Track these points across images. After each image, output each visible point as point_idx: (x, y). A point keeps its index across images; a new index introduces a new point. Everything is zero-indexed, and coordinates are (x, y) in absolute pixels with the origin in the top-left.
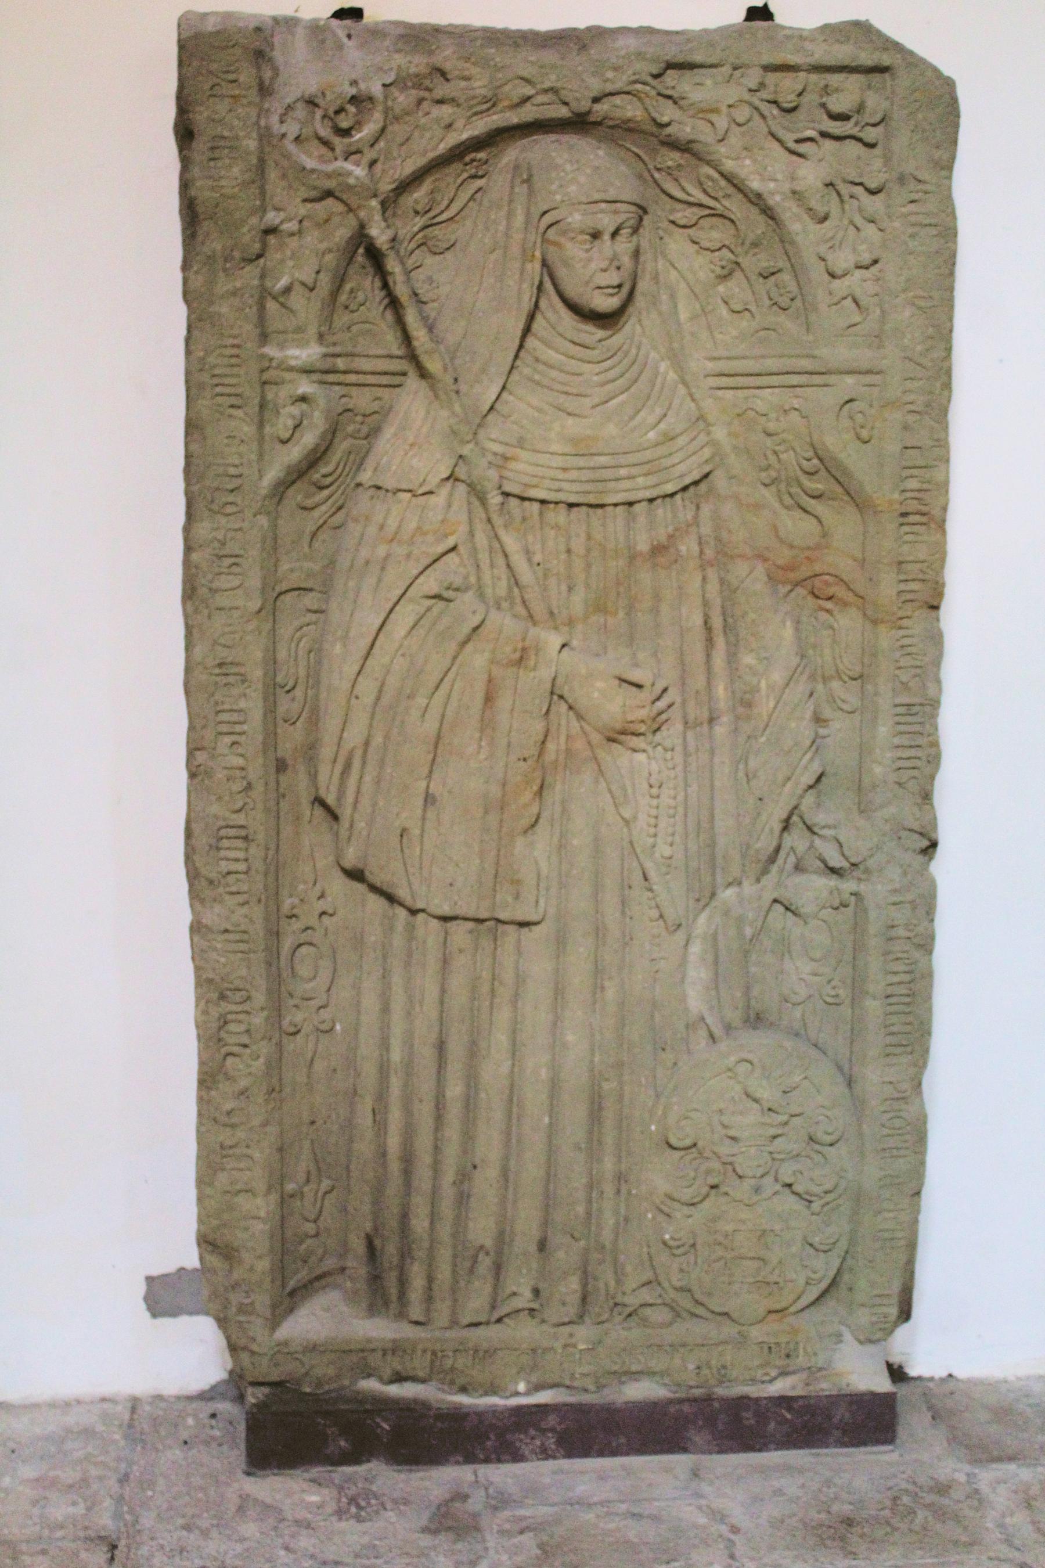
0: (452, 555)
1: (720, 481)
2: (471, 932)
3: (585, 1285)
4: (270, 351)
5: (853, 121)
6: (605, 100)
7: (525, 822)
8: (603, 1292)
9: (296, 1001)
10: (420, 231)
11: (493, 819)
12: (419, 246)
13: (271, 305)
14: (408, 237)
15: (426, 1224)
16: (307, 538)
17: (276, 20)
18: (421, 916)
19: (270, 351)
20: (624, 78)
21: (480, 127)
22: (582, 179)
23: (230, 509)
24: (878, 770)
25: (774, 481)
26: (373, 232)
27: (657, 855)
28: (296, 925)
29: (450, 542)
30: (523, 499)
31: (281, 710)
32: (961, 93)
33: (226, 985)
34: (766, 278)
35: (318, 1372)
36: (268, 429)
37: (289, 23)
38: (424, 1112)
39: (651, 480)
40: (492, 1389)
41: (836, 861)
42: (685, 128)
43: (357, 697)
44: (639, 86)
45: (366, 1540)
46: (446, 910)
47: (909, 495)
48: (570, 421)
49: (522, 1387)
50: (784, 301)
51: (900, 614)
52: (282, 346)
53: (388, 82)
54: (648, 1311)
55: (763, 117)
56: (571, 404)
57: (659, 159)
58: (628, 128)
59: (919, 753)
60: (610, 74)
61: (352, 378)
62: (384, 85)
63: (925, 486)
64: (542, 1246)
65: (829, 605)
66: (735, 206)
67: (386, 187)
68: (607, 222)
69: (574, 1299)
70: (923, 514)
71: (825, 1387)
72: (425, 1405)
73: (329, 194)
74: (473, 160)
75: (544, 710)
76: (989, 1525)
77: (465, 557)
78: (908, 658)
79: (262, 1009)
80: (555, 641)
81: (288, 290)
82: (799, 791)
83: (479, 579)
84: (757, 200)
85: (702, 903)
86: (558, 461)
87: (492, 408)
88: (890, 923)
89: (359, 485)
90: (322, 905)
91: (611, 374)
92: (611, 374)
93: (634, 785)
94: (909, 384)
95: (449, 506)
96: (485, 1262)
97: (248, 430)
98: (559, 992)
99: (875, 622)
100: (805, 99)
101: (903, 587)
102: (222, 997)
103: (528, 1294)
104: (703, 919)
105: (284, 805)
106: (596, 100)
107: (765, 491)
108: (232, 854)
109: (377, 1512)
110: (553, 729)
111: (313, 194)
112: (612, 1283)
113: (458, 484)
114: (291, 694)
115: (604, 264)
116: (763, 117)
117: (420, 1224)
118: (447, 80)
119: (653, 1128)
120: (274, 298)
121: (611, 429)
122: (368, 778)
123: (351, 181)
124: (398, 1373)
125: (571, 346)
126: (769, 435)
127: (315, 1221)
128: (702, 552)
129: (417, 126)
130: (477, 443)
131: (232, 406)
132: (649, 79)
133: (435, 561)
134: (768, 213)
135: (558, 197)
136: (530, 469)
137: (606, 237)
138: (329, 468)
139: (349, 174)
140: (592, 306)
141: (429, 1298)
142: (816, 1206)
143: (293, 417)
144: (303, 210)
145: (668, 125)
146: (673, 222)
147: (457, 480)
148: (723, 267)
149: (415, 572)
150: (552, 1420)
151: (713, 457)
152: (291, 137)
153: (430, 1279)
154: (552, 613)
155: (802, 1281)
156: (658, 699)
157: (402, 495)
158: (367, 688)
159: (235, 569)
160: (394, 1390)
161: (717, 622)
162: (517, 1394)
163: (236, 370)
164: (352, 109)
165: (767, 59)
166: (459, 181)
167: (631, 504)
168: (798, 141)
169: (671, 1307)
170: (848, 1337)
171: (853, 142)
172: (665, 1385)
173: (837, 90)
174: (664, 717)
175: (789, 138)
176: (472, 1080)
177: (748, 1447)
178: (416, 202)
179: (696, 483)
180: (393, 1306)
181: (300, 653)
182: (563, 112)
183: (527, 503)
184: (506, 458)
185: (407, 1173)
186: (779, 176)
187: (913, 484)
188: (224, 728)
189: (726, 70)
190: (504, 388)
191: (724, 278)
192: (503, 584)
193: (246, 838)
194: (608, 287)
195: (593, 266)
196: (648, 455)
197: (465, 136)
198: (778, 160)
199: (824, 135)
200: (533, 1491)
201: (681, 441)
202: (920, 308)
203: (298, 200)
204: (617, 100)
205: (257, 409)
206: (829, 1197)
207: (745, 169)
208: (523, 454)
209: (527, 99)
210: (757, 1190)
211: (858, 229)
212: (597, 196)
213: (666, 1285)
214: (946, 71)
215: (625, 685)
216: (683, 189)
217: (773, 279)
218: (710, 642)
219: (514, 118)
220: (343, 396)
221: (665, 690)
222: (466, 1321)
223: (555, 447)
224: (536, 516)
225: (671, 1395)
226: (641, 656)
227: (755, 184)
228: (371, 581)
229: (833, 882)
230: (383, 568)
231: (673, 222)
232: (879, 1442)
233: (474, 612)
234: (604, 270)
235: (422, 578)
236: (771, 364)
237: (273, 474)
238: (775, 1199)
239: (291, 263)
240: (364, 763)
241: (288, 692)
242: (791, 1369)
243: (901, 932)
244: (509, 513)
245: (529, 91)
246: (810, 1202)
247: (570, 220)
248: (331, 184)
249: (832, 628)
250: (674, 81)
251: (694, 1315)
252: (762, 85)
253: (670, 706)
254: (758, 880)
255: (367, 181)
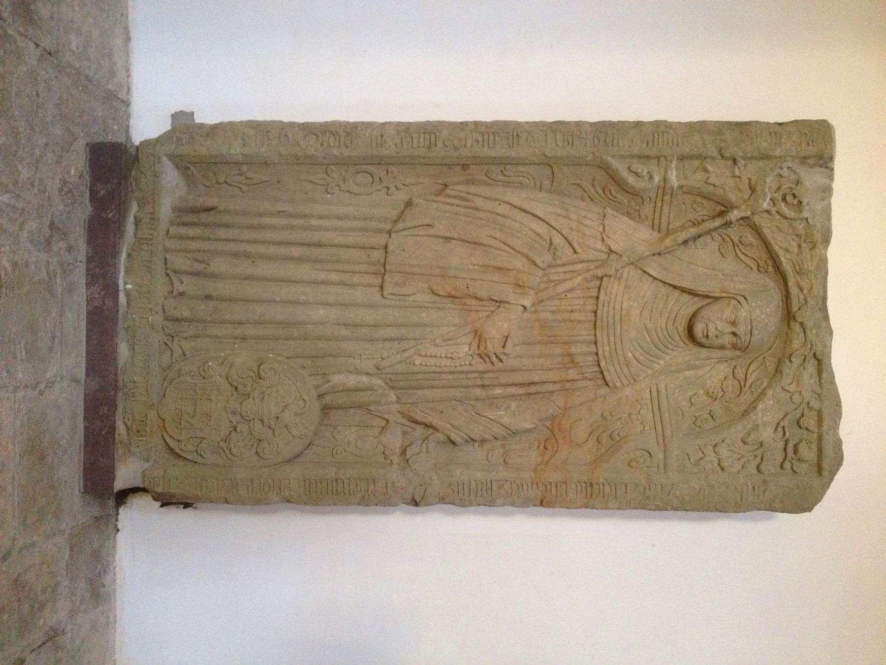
0: (572, 251)
1: (604, 391)
2: (379, 261)
3: (186, 320)
4: (674, 162)
5: (794, 456)
6: (802, 329)
7: (435, 288)
8: (181, 329)
9: (343, 173)
10: (732, 240)
11: (437, 272)
12: (723, 239)
13: (697, 163)
14: (729, 234)
15: (223, 237)
16: (577, 182)
17: (832, 169)
18: (387, 236)
19: (674, 162)
20: (813, 339)
21: (787, 266)
22: (763, 317)
23: (596, 140)
24: (458, 472)
25: (605, 419)
26: (735, 212)
27: (415, 357)
28: (383, 174)
29: (579, 250)
30: (599, 288)
31: (492, 167)
32: (806, 514)
33: (354, 136)
34: (710, 414)
35: (143, 180)
36: (635, 160)
37: (831, 177)
38: (285, 236)
39: (607, 354)
40: (127, 272)
41: (409, 453)
42: (789, 369)
43: (500, 204)
44: (809, 346)
45: (48, 188)
46: (391, 248)
47: (602, 487)
48: (638, 312)
49: (129, 286)
50: (698, 423)
51: (540, 484)
52: (677, 168)
53: (809, 220)
54: (169, 353)
55: (796, 409)
56: (646, 313)
57: (770, 358)
58: (788, 340)
59: (467, 494)
60: (814, 331)
61: (659, 204)
62: (807, 218)
63: (606, 496)
64: (208, 297)
65: (542, 447)
66: (747, 398)
67: (757, 219)
68: (741, 330)
69: (177, 314)
70: (591, 495)
71: (120, 452)
72: (121, 236)
73: (753, 191)
74: (768, 265)
75: (493, 298)
76: (35, 538)
77: (571, 258)
78: (516, 488)
79: (341, 154)
80: (527, 303)
81: (706, 170)
82: (447, 432)
83: (558, 266)
84: (752, 407)
85: (390, 383)
86: (618, 306)
87: (644, 272)
88: (376, 480)
89: (605, 208)
90: (393, 189)
91: (660, 334)
92: (660, 334)
93: (452, 345)
94: (659, 487)
95: (596, 250)
96: (200, 267)
97: (636, 150)
98: (346, 305)
99: (535, 470)
100: (804, 432)
101: (554, 485)
102: (348, 134)
103: (181, 290)
104: (380, 382)
105: (445, 168)
106: (802, 324)
107: (599, 414)
108: (422, 139)
109: (63, 201)
110: (483, 303)
111: (753, 183)
112: (185, 335)
113: (607, 255)
114: (500, 173)
115: (719, 328)
116: (796, 409)
117: (223, 233)
118: (811, 249)
119: (271, 356)
120: (701, 164)
121: (633, 334)
122: (459, 209)
123: (761, 201)
124: (140, 221)
125: (675, 314)
126: (629, 415)
127: (225, 182)
128: (568, 381)
129: (787, 235)
130: (628, 264)
131: (648, 142)
132: (813, 351)
133: (569, 243)
134: (746, 413)
135: (754, 304)
136: (614, 291)
137: (733, 329)
138: (613, 193)
139: (764, 200)
140: (697, 323)
141: (181, 238)
142: (222, 444)
143: (642, 172)
144: (745, 179)
145: (790, 361)
146: (735, 367)
147: (609, 254)
148: (713, 393)
149: (564, 232)
150: (109, 303)
151: (616, 387)
152: (781, 172)
153: (192, 239)
154: (541, 302)
155: (181, 438)
156: (497, 357)
157: (602, 227)
158: (503, 209)
159: (566, 143)
160: (131, 219)
161: (533, 389)
162: (125, 283)
163: (665, 143)
164: (796, 202)
165: (825, 411)
166: (756, 259)
167: (596, 343)
168: (783, 427)
169: (170, 367)
170: (147, 465)
171: (783, 457)
172: (126, 364)
173: (810, 448)
174: (487, 360)
175: (784, 423)
176: (300, 260)
177: (86, 410)
178: (747, 237)
179: (604, 379)
180: (178, 220)
181: (521, 178)
182: (795, 308)
183: (597, 290)
184: (620, 279)
185: (251, 227)
186: (765, 419)
187: (607, 489)
188: (486, 137)
189: (818, 390)
190: (655, 278)
191: (707, 394)
192: (555, 277)
193: (430, 147)
194: (707, 331)
195: (718, 323)
196: (620, 352)
197: (783, 259)
198: (772, 417)
199: (787, 442)
200: (70, 289)
201: (625, 370)
202: (699, 493)
203: (749, 176)
204: (802, 335)
205: (646, 154)
206: (227, 452)
207: (768, 401)
208: (622, 287)
209: (801, 290)
210: (234, 413)
211: (739, 460)
212: (754, 324)
213: (182, 364)
214: (816, 508)
215: (505, 339)
216: (754, 371)
217: (709, 417)
218: (522, 385)
219: (791, 283)
220: (650, 198)
221: (501, 360)
222: (168, 256)
223: (625, 305)
224: (590, 294)
225: (120, 367)
226: (518, 348)
227: (760, 406)
228: (559, 211)
229: (398, 451)
230: (565, 217)
231: (735, 367)
232: (85, 486)
233: (543, 262)
234: (716, 328)
235: (560, 236)
236: (666, 416)
237: (615, 163)
238: (228, 422)
239: (718, 172)
240: (465, 207)
241: (502, 171)
242: (131, 434)
243: (371, 487)
244: (592, 280)
245: (805, 291)
246: (225, 442)
247: (743, 310)
248: (759, 189)
249: (530, 448)
250: (811, 366)
251: (165, 379)
252: (811, 409)
253: (492, 363)
254: (398, 412)
255: (761, 209)
